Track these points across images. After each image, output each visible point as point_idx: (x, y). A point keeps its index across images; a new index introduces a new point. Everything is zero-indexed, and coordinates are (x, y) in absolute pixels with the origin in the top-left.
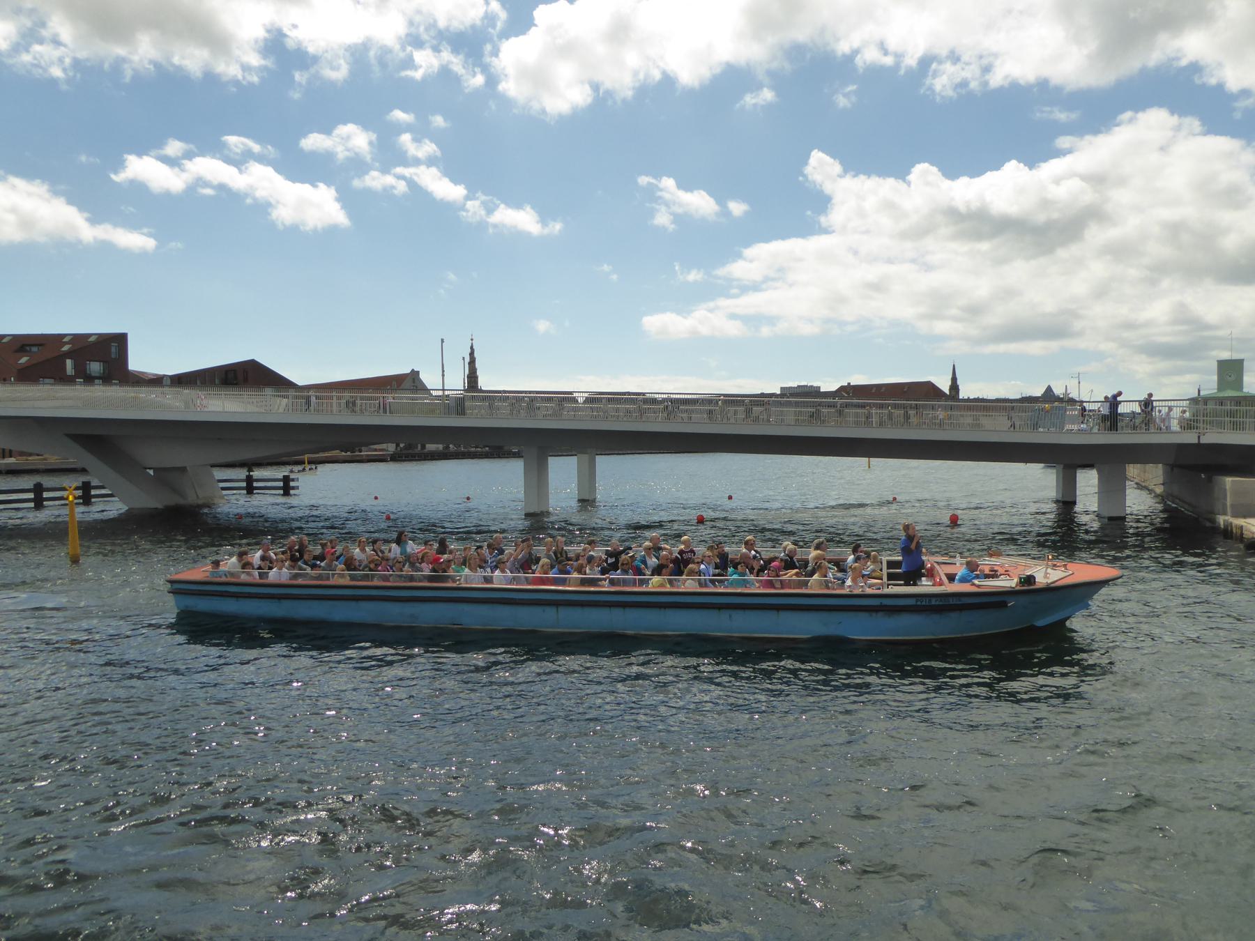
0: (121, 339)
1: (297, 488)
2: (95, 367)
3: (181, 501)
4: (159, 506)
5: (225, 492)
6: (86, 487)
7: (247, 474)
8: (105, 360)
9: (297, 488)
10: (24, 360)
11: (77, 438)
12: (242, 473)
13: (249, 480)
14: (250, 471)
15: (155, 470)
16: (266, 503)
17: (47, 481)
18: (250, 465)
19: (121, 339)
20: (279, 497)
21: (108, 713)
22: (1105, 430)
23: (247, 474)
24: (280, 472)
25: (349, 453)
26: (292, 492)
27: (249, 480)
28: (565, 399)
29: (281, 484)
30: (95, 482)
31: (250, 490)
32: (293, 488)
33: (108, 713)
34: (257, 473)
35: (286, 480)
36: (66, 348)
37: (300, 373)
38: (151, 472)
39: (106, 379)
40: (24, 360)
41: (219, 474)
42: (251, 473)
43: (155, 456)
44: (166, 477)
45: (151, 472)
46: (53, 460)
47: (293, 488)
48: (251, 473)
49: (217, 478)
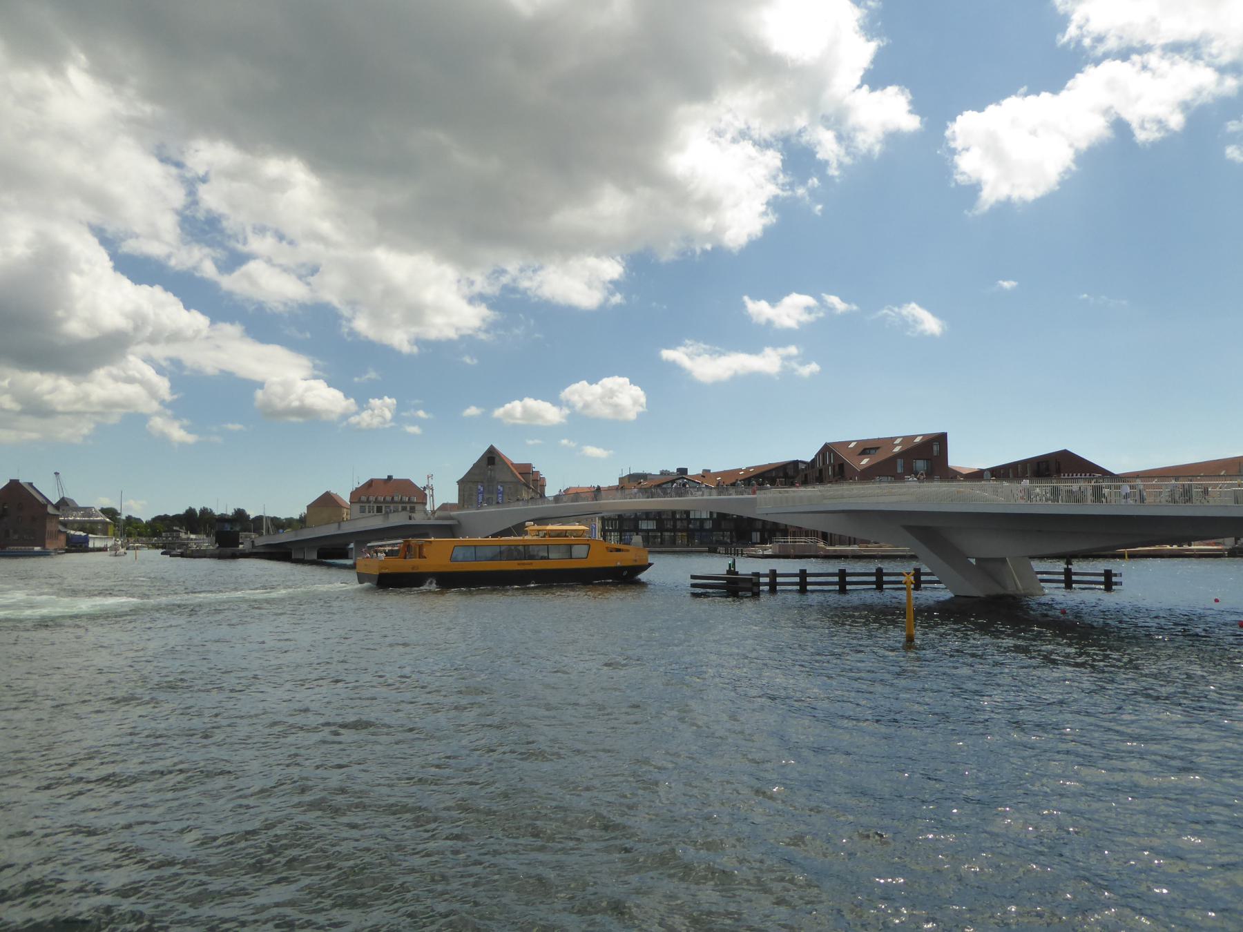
0: (942, 439)
1: (1121, 584)
2: (920, 465)
3: (1000, 591)
4: (982, 595)
5: (1042, 584)
6: (918, 573)
7: (1066, 566)
8: (929, 459)
9: (1121, 584)
10: (865, 461)
11: (911, 529)
12: (1060, 566)
13: (1068, 573)
14: (1069, 563)
15: (978, 560)
16: (1087, 598)
17: (887, 567)
18: (1069, 558)
19: (942, 439)
20: (832, 595)
21: (107, 763)
22: (831, 534)
23: (1066, 566)
24: (1100, 566)
25: (1175, 547)
26: (1114, 587)
27: (1068, 573)
28: (679, 480)
29: (873, 579)
30: (924, 569)
31: (1069, 584)
32: (1116, 584)
33: (107, 763)
34: (1077, 566)
35: (1108, 574)
36: (897, 449)
37: (1116, 463)
38: (973, 561)
39: (930, 475)
40: (865, 461)
41: (1037, 566)
42: (1070, 567)
43: (982, 546)
44: (989, 567)
45: (973, 561)
46: (887, 548)
47: (1116, 584)
48: (1070, 567)
49: (1036, 570)
